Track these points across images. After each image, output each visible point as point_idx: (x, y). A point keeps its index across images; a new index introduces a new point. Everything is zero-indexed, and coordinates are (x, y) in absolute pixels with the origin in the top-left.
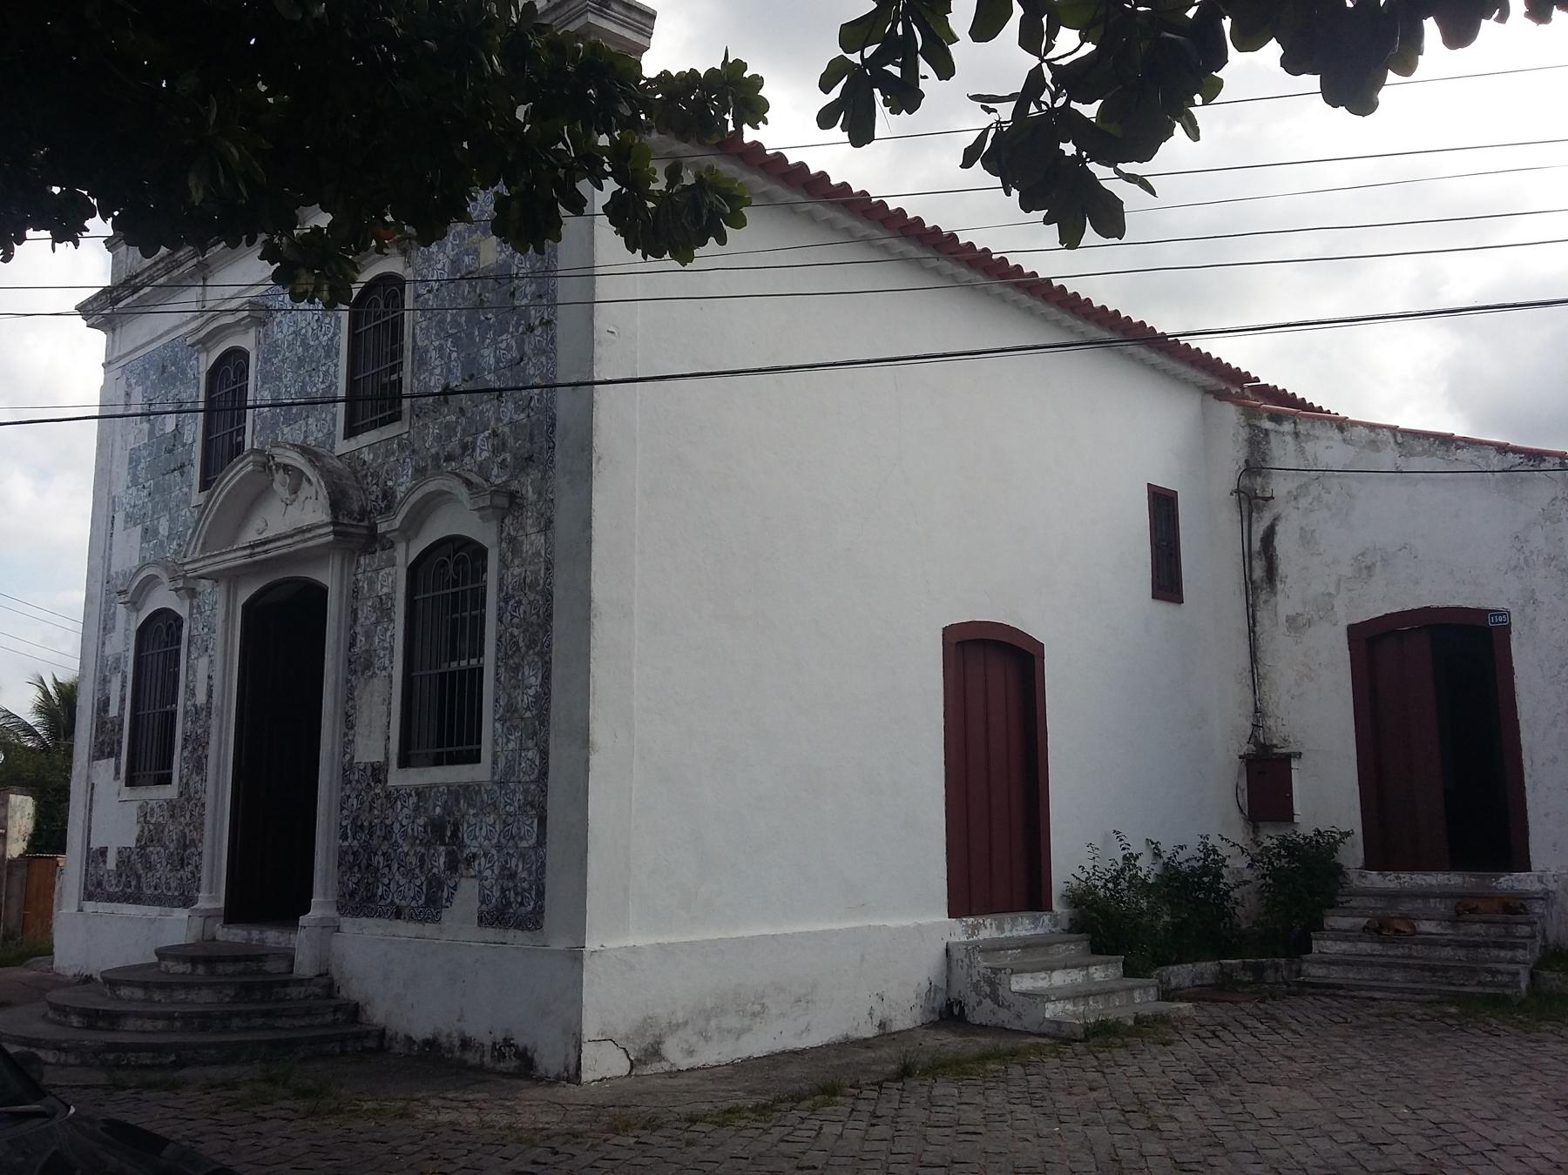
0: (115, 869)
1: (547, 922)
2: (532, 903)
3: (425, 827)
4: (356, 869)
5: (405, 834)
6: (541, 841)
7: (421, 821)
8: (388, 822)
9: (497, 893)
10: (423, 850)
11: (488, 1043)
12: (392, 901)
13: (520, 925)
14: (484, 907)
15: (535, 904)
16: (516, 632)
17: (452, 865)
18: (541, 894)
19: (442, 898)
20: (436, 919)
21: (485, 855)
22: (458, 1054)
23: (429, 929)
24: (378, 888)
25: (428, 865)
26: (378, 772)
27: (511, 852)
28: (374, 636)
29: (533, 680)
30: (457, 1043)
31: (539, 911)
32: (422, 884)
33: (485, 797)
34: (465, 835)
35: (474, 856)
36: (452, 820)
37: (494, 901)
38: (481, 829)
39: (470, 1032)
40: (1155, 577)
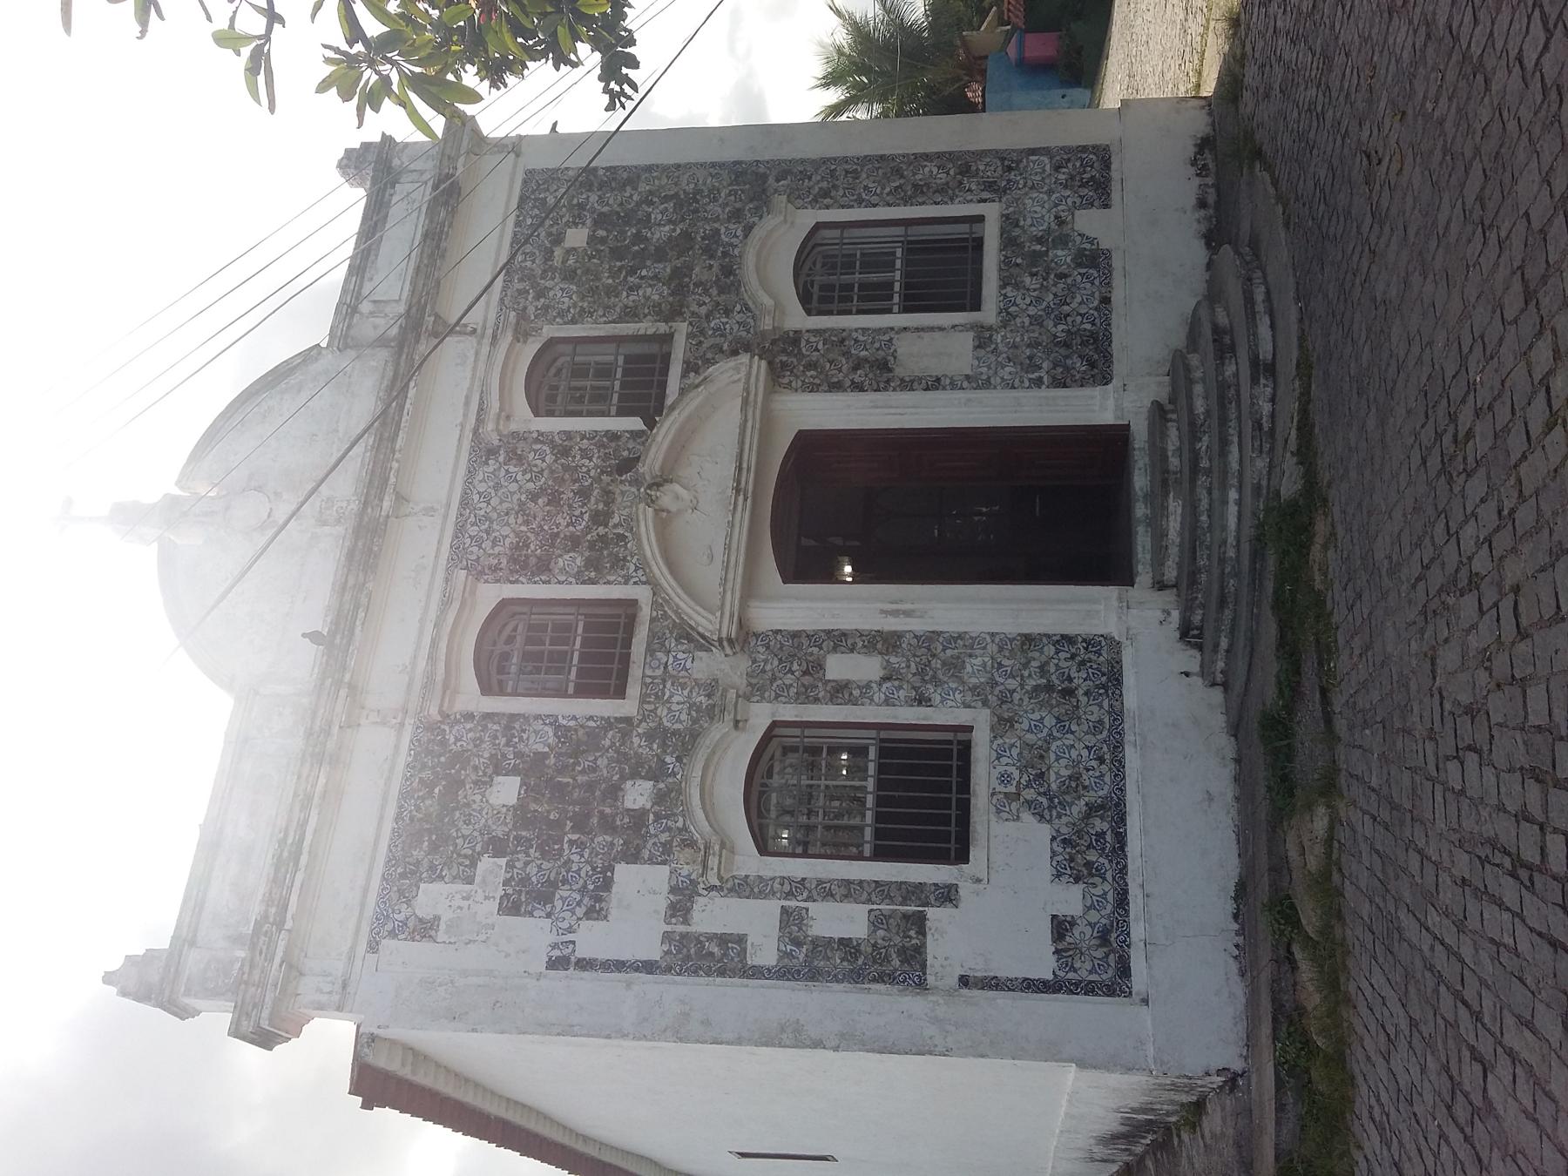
0: (1081, 886)
1: (1102, 141)
2: (1091, 156)
3: (1033, 275)
4: (1069, 362)
5: (1039, 300)
6: (1045, 151)
7: (1027, 280)
8: (1027, 321)
9: (1084, 191)
10: (1052, 276)
11: (1197, 181)
12: (1096, 309)
13: (1107, 164)
14: (1096, 203)
15: (1091, 153)
16: (888, 190)
17: (1063, 241)
18: (1084, 149)
19: (1090, 250)
20: (1107, 254)
21: (1056, 205)
22: (1211, 211)
23: (1117, 262)
24: (1085, 330)
25: (1063, 269)
26: (983, 337)
27: (1054, 180)
28: (858, 358)
29: (927, 169)
30: (1202, 213)
31: (1096, 149)
32: (1080, 274)
33: (1011, 209)
34: (1041, 228)
35: (1056, 217)
36: (1028, 244)
37: (1091, 194)
38: (1036, 212)
39: (1193, 201)
40: (843, 852)
